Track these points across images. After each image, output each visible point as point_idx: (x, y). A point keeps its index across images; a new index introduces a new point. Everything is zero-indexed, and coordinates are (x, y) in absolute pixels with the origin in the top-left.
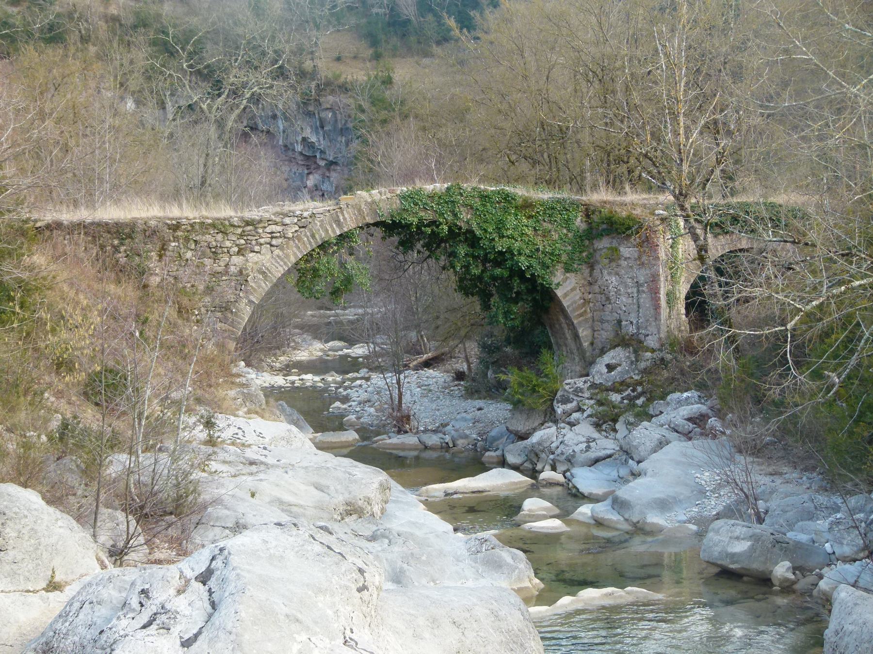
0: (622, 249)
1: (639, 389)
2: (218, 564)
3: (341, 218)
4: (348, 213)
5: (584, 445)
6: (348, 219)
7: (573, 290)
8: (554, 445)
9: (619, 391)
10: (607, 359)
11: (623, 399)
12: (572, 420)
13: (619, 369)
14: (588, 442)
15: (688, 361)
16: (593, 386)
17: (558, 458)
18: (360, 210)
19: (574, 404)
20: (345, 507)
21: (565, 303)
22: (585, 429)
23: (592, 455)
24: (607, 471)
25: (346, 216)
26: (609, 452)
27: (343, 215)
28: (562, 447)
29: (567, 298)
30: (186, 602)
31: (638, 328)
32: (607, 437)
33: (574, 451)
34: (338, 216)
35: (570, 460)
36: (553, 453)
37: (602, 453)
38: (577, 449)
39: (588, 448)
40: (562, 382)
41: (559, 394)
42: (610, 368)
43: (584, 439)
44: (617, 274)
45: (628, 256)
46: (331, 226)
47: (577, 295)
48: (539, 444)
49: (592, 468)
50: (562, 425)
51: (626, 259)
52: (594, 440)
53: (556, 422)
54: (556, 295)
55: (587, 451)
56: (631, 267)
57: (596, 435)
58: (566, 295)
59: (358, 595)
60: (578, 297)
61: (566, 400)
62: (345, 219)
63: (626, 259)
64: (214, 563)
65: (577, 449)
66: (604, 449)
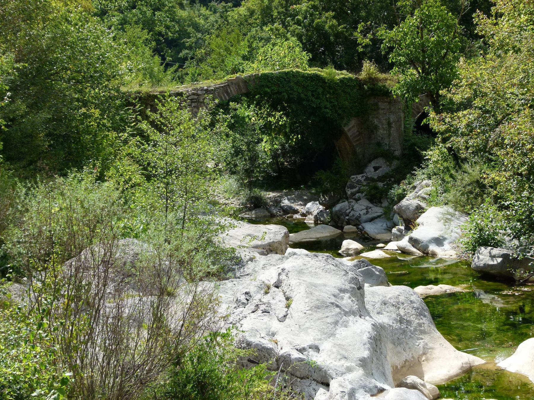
0: (380, 104)
1: (393, 179)
2: (283, 277)
3: (229, 90)
4: (233, 88)
5: (365, 211)
6: (233, 91)
7: (353, 127)
8: (348, 211)
9: (383, 182)
10: (373, 164)
11: (384, 185)
12: (357, 197)
13: (381, 169)
14: (367, 209)
15: (213, 177)
16: (367, 179)
17: (351, 218)
18: (239, 86)
19: (357, 188)
20: (269, 247)
21: (349, 134)
22: (364, 203)
23: (370, 216)
24: (380, 224)
25: (232, 89)
26: (379, 214)
27: (230, 89)
28: (352, 213)
29: (350, 131)
30: (281, 298)
31: (389, 147)
32: (377, 206)
33: (360, 214)
34: (227, 90)
35: (358, 219)
36: (348, 215)
37: (375, 215)
38: (362, 213)
39: (367, 212)
40: (349, 177)
41: (348, 183)
42: (376, 169)
43: (365, 208)
44: (377, 118)
45: (383, 108)
46: (224, 95)
47: (355, 130)
48: (340, 211)
49: (372, 222)
50: (351, 200)
51: (382, 109)
52: (370, 208)
53: (347, 199)
54: (344, 130)
55: (367, 214)
56: (385, 114)
57: (371, 205)
58: (349, 130)
59: (358, 291)
60: (356, 131)
61: (352, 187)
62: (231, 91)
63: (382, 109)
64: (281, 277)
65: (362, 213)
66: (376, 212)
